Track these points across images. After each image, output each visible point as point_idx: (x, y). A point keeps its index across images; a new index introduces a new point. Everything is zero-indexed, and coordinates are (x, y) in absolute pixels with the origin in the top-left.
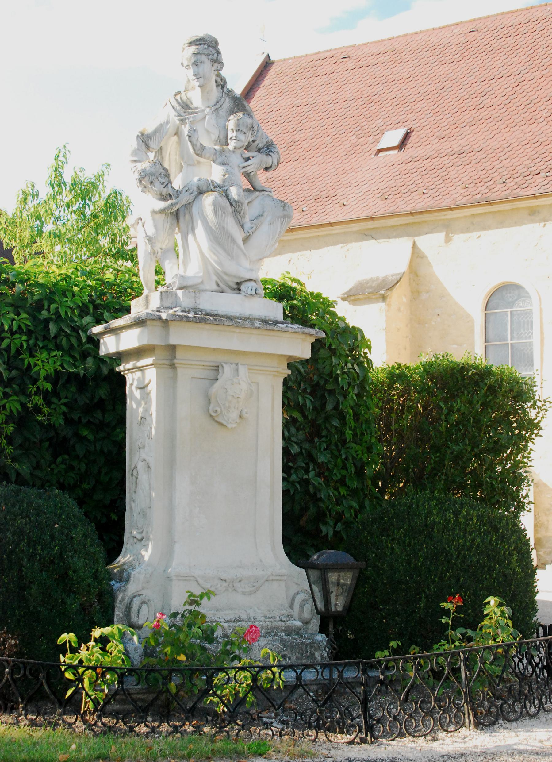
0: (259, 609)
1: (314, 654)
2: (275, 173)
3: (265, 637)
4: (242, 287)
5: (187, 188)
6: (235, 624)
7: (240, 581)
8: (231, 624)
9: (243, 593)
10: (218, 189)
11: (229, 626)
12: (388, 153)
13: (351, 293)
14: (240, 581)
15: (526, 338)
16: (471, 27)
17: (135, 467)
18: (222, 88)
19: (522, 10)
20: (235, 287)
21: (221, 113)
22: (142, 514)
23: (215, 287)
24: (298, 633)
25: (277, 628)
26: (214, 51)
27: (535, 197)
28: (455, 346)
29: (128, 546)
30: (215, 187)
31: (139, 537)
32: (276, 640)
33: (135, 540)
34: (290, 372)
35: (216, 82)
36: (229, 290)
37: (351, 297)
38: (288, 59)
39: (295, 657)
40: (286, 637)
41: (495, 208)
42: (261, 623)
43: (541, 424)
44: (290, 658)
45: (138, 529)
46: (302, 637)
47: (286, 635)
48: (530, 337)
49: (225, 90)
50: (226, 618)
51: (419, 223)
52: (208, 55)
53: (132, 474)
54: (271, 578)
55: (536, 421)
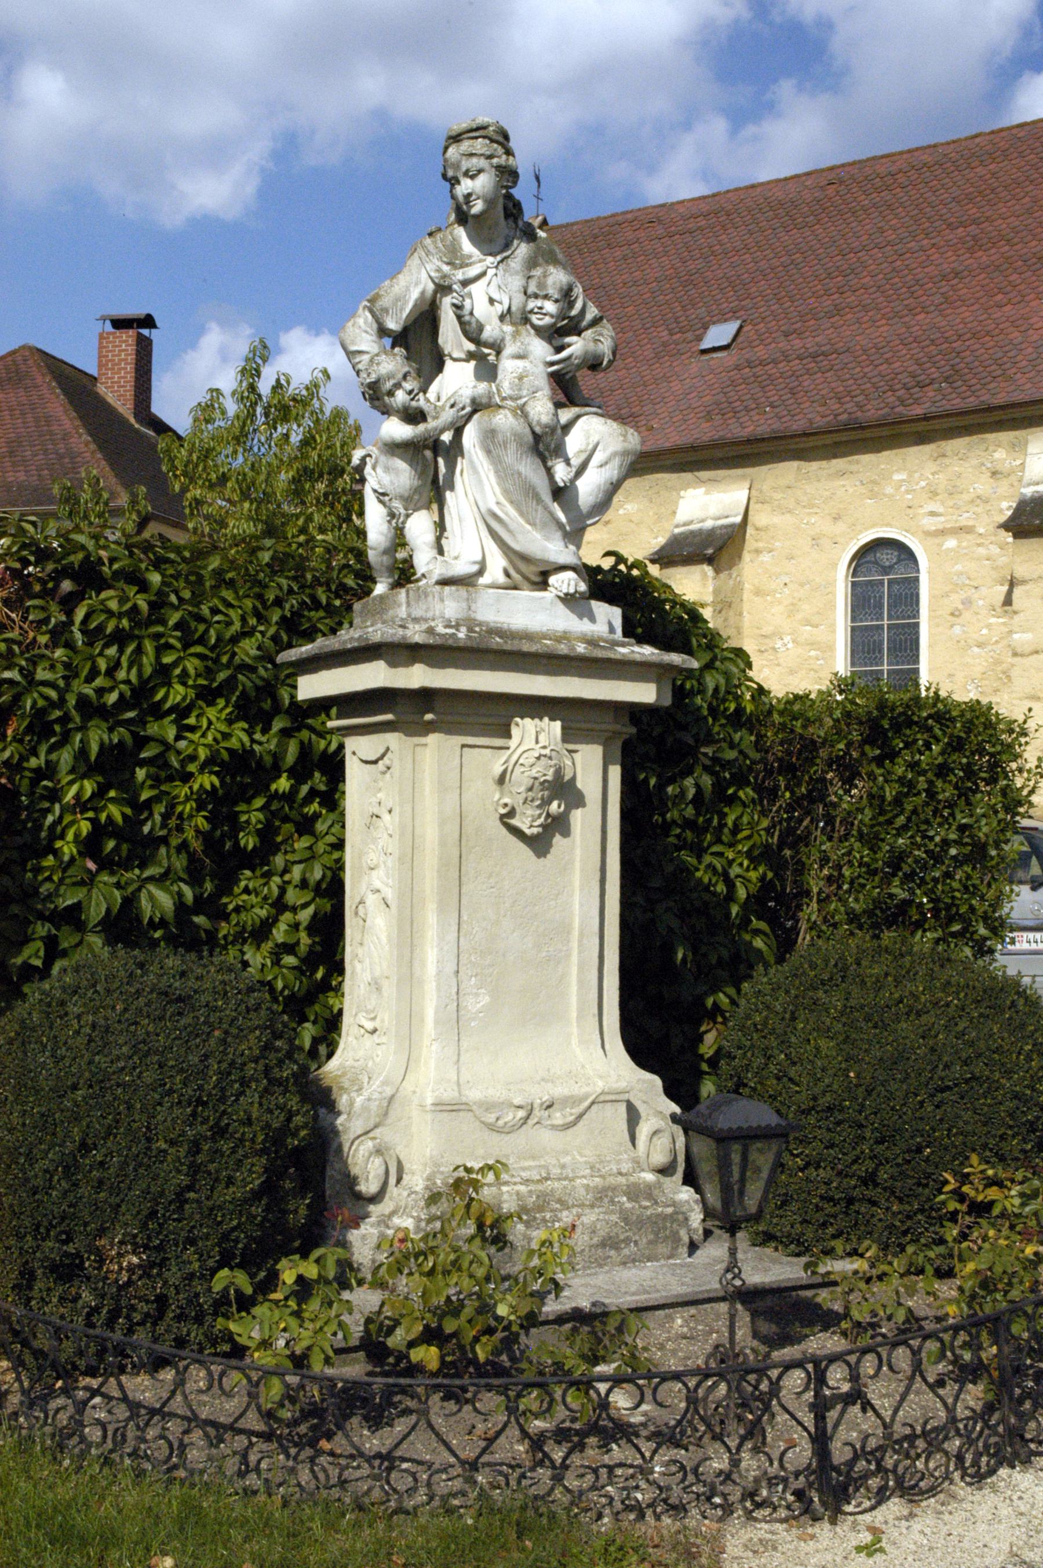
0: (581, 1155)
1: (678, 1232)
2: (611, 375)
3: (592, 1206)
4: (552, 580)
5: (452, 401)
6: (540, 1187)
7: (549, 1107)
8: (532, 1187)
9: (554, 1127)
10: (509, 403)
11: (530, 1191)
12: (715, 355)
13: (664, 553)
14: (549, 1107)
15: (909, 618)
16: (831, 176)
17: (362, 902)
18: (516, 222)
19: (901, 153)
20: (537, 579)
21: (513, 265)
22: (374, 987)
23: (502, 579)
24: (650, 1196)
25: (614, 1189)
26: (500, 150)
27: (926, 418)
28: (808, 628)
29: (350, 1039)
30: (504, 399)
31: (369, 1025)
32: (612, 1212)
33: (362, 1031)
34: (633, 730)
35: (505, 208)
36: (526, 584)
37: (666, 557)
38: (573, 224)
39: (645, 1240)
40: (628, 1205)
41: (868, 434)
42: (585, 1182)
43: (1034, 799)
44: (636, 1243)
45: (367, 1012)
46: (656, 1203)
47: (629, 1199)
48: (914, 617)
49: (520, 223)
50: (523, 1174)
51: (747, 455)
52: (490, 157)
53: (356, 914)
54: (602, 1098)
55: (1025, 793)
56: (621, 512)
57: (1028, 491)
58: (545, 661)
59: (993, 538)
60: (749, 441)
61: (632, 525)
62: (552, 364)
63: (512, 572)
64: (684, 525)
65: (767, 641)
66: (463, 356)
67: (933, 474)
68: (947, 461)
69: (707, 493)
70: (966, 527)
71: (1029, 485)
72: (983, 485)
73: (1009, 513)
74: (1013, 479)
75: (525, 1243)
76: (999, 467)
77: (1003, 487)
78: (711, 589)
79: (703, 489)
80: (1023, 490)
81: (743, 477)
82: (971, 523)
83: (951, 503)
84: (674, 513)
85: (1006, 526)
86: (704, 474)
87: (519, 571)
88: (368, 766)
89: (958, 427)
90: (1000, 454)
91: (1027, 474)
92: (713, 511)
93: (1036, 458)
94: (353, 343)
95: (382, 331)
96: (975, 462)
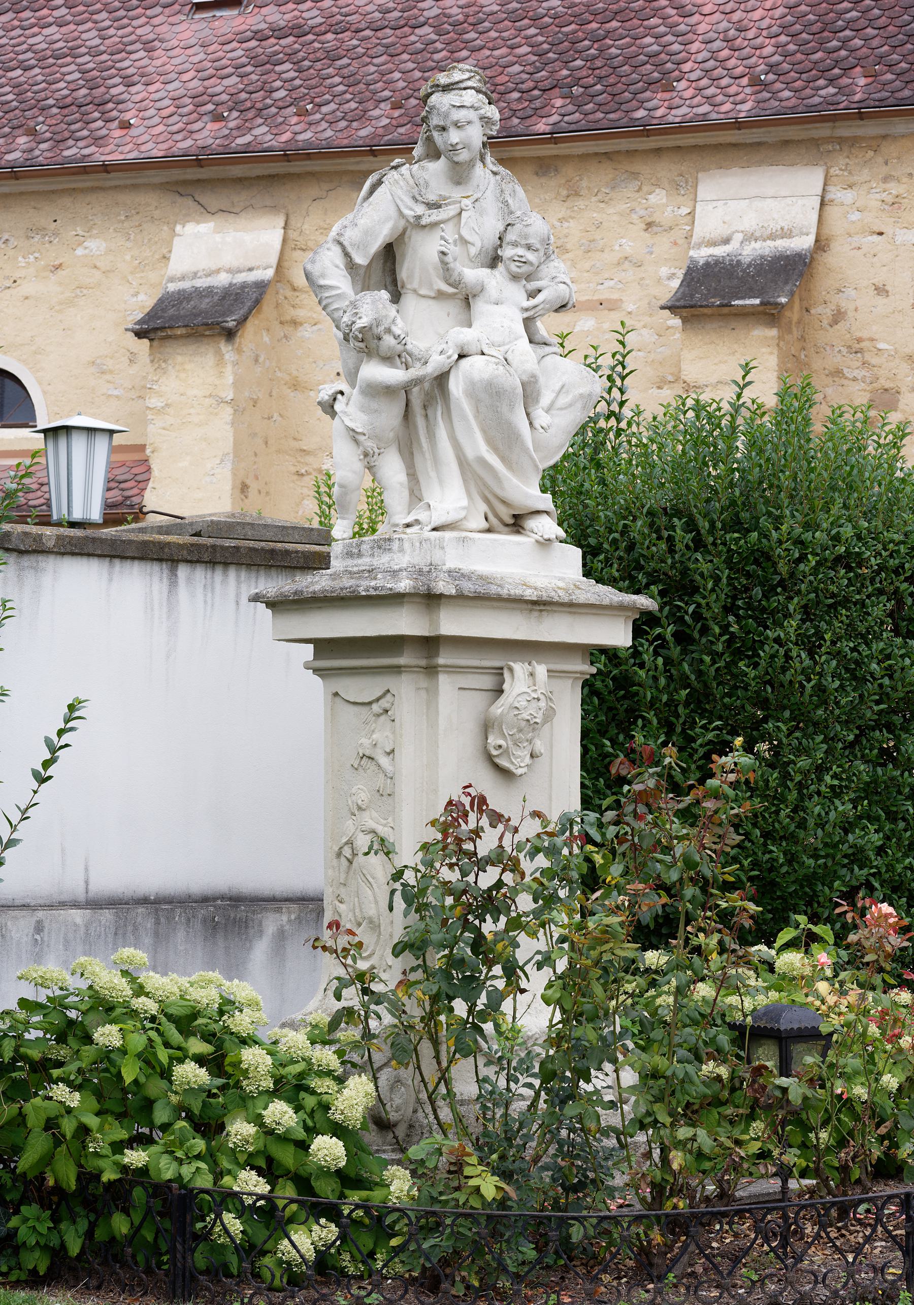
4: (531, 523)
20: (511, 521)
23: (484, 525)
36: (501, 528)
56: (79, 252)
57: (702, 254)
58: (530, 606)
59: (647, 319)
60: (286, 157)
61: (97, 274)
62: (527, 310)
63: (491, 516)
64: (183, 278)
65: (309, 459)
66: (433, 294)
67: (560, 220)
68: (581, 203)
69: (216, 231)
70: (609, 300)
71: (699, 246)
72: (632, 242)
73: (676, 283)
74: (678, 235)
75: (718, 1086)
76: (657, 218)
77: (663, 244)
78: (230, 379)
79: (211, 225)
80: (692, 253)
81: (274, 209)
82: (615, 296)
83: (587, 265)
84: (166, 258)
85: (672, 308)
86: (210, 200)
87: (497, 516)
88: (356, 709)
89: (596, 154)
90: (658, 197)
91: (697, 229)
92: (229, 259)
93: (710, 207)
94: (323, 276)
95: (351, 266)
96: (623, 207)
